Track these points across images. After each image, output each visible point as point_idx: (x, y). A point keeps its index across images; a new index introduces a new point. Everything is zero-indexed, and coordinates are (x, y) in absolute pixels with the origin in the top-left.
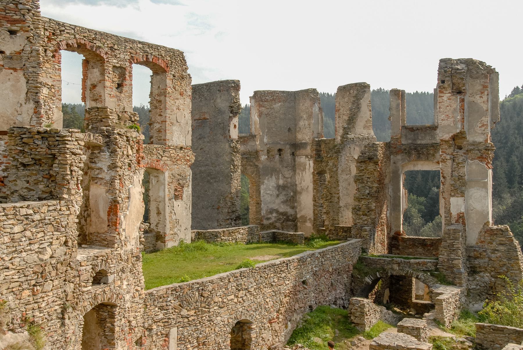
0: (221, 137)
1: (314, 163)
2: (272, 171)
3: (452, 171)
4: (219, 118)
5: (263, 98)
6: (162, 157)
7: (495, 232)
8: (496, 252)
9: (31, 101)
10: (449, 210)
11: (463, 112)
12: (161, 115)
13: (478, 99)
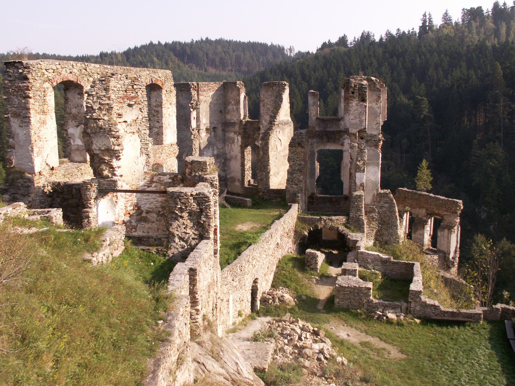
0: (183, 127)
4: (181, 112)
7: (383, 195)
9: (144, 154)
12: (158, 122)
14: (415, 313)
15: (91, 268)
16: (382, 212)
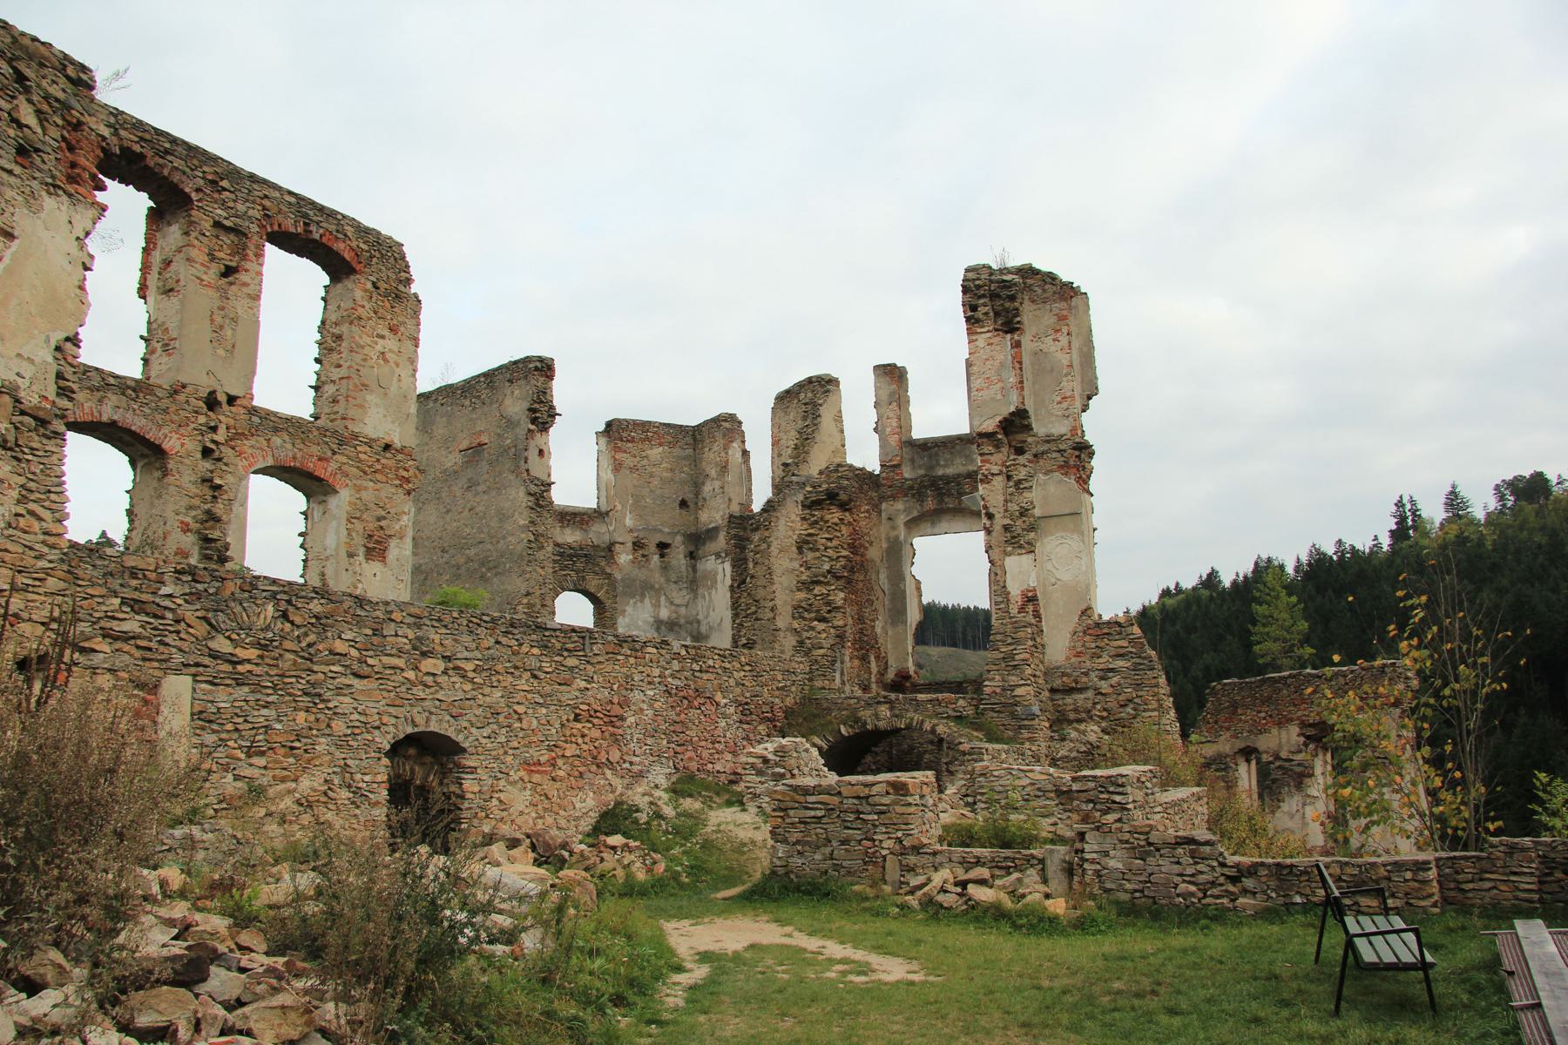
1: (733, 566)
2: (644, 589)
3: (1006, 501)
5: (624, 435)
8: (1111, 674)
10: (1004, 587)
11: (1021, 369)
13: (1048, 344)
14: (1109, 885)
15: (343, 998)
16: (1110, 690)
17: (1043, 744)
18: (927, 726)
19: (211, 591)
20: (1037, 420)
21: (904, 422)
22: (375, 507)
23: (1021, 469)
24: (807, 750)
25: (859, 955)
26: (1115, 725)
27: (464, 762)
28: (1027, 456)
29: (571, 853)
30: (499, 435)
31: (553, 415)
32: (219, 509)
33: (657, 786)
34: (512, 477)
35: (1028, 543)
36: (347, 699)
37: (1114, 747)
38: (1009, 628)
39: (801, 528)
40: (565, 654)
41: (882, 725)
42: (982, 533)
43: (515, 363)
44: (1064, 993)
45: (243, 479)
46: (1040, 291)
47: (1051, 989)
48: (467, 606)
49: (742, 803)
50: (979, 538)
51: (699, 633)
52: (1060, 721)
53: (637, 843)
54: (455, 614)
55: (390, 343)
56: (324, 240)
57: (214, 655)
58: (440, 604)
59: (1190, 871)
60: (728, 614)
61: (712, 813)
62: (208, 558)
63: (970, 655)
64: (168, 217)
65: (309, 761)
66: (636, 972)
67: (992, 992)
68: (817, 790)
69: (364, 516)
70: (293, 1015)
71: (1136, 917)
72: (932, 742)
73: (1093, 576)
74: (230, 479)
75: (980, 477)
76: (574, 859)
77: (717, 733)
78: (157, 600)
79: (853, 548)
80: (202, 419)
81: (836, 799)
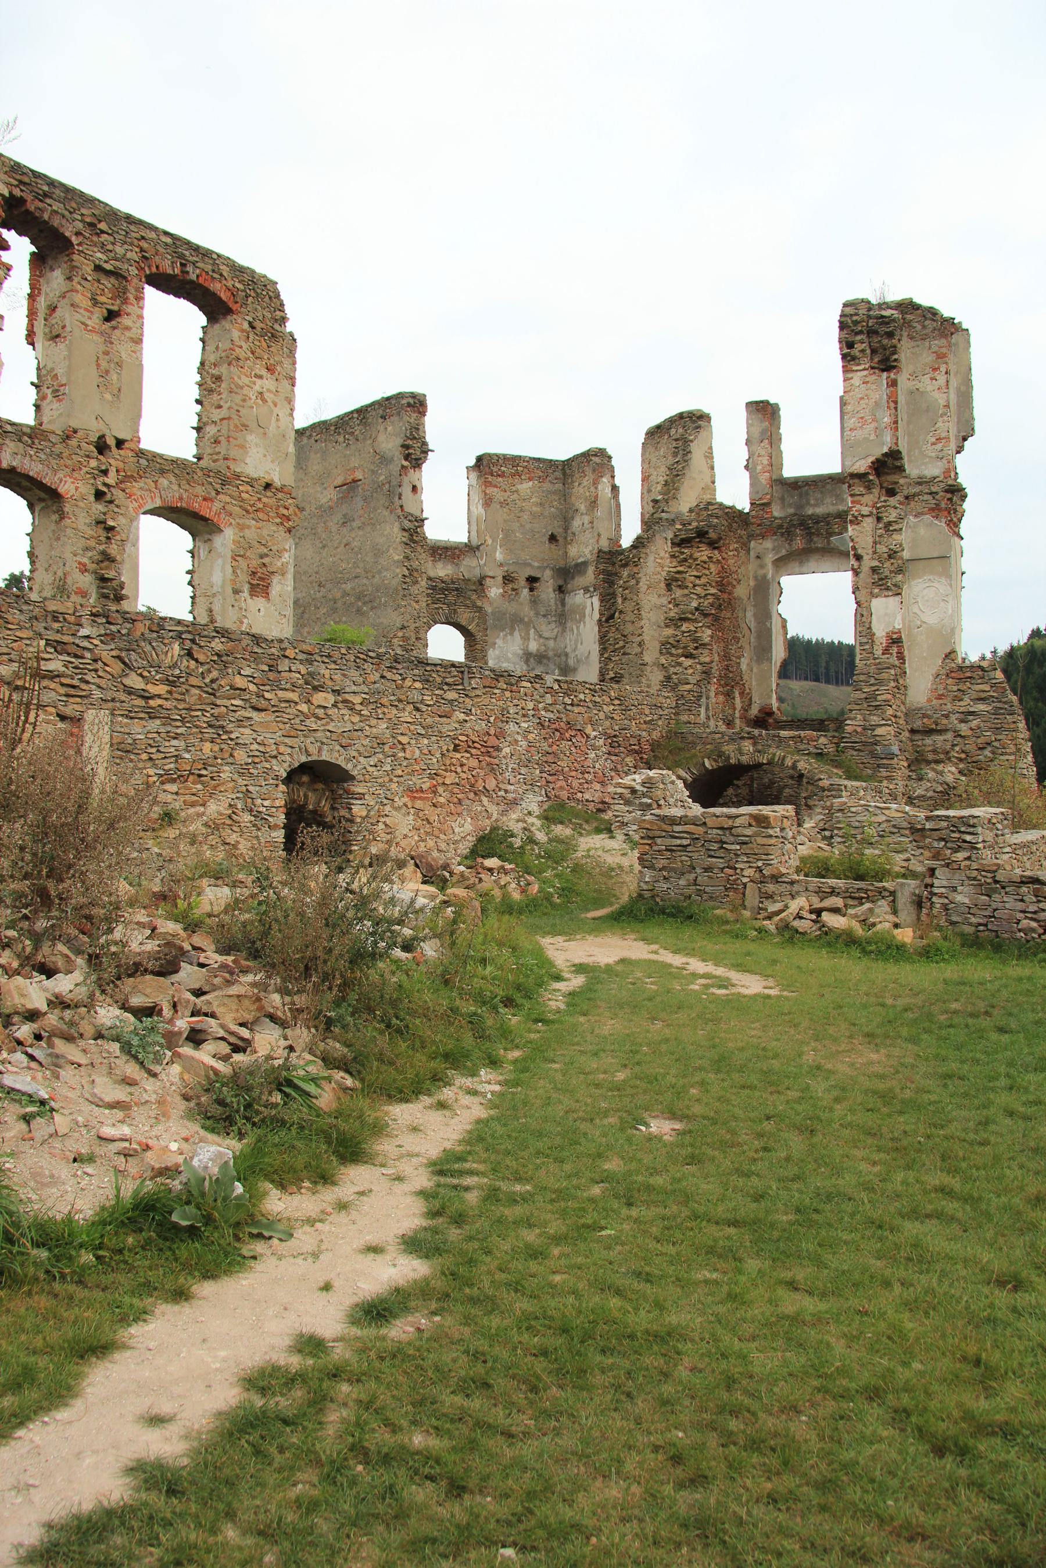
1: (602, 601)
2: (514, 622)
3: (875, 543)
5: (495, 469)
6: (218, 493)
10: (870, 628)
11: (896, 409)
13: (926, 384)
14: (954, 919)
15: (283, 991)
16: (969, 733)
17: (900, 783)
18: (789, 762)
19: (124, 632)
20: (910, 461)
21: (775, 460)
22: (257, 545)
23: (891, 510)
24: (673, 782)
25: (720, 971)
26: (972, 766)
27: (353, 788)
28: (898, 497)
29: (451, 873)
30: (373, 471)
31: (425, 451)
32: (113, 550)
33: (529, 813)
34: (386, 513)
35: (895, 585)
36: (247, 731)
37: (971, 789)
38: (872, 670)
39: (669, 566)
40: (446, 687)
41: (745, 759)
42: (850, 574)
43: (388, 399)
44: (906, 1010)
45: (133, 520)
46: (919, 327)
47: (894, 1006)
48: (353, 642)
49: (610, 831)
50: (846, 578)
51: (567, 665)
52: (918, 761)
53: (512, 866)
54: (343, 651)
55: (268, 383)
56: (201, 281)
57: (130, 691)
58: (329, 640)
59: (1032, 908)
60: (595, 648)
61: (582, 840)
62: (106, 597)
63: (832, 690)
64: (50, 262)
65: (215, 788)
66: (522, 979)
67: (841, 1007)
68: (682, 820)
69: (248, 554)
70: (246, 1002)
71: (978, 948)
72: (792, 777)
73: (959, 620)
74: (122, 520)
75: (850, 517)
76: (455, 879)
77: (586, 764)
78: (77, 641)
79: (722, 586)
80: (94, 463)
81: (701, 830)
